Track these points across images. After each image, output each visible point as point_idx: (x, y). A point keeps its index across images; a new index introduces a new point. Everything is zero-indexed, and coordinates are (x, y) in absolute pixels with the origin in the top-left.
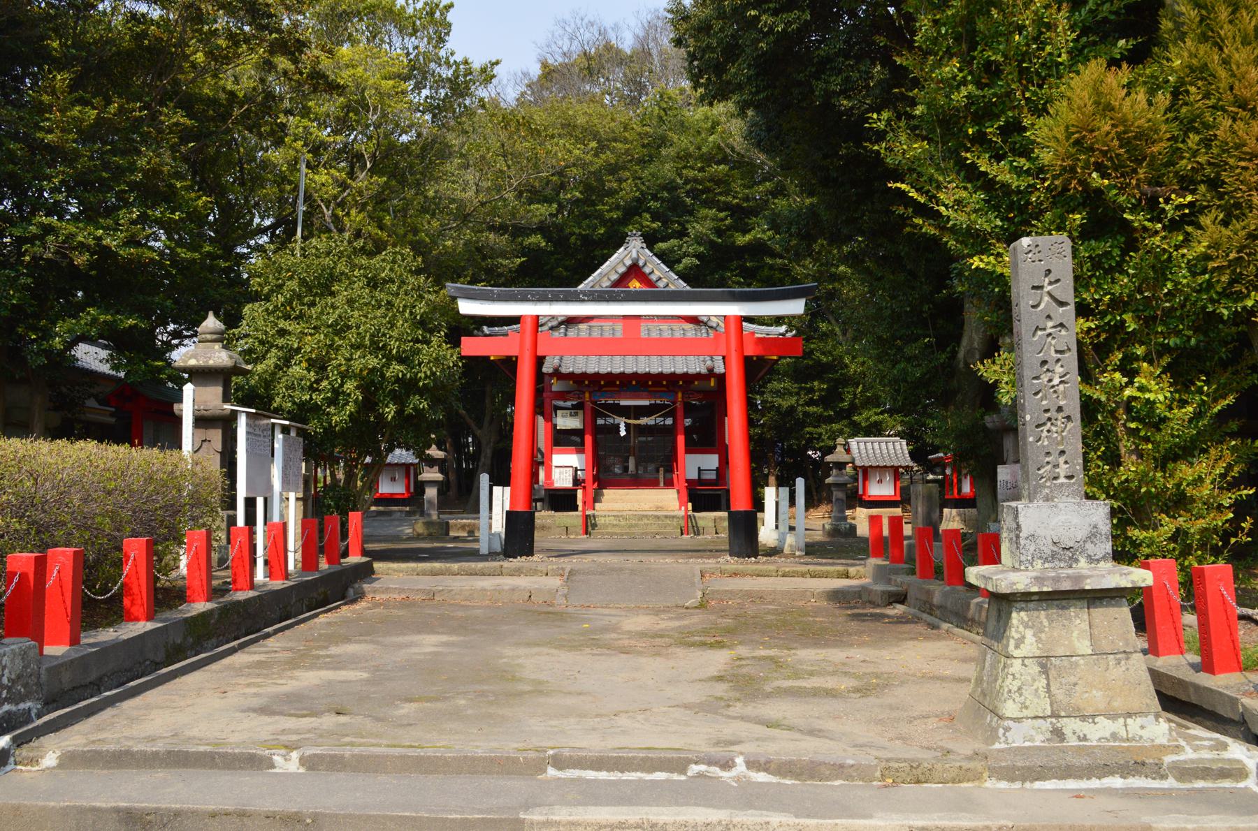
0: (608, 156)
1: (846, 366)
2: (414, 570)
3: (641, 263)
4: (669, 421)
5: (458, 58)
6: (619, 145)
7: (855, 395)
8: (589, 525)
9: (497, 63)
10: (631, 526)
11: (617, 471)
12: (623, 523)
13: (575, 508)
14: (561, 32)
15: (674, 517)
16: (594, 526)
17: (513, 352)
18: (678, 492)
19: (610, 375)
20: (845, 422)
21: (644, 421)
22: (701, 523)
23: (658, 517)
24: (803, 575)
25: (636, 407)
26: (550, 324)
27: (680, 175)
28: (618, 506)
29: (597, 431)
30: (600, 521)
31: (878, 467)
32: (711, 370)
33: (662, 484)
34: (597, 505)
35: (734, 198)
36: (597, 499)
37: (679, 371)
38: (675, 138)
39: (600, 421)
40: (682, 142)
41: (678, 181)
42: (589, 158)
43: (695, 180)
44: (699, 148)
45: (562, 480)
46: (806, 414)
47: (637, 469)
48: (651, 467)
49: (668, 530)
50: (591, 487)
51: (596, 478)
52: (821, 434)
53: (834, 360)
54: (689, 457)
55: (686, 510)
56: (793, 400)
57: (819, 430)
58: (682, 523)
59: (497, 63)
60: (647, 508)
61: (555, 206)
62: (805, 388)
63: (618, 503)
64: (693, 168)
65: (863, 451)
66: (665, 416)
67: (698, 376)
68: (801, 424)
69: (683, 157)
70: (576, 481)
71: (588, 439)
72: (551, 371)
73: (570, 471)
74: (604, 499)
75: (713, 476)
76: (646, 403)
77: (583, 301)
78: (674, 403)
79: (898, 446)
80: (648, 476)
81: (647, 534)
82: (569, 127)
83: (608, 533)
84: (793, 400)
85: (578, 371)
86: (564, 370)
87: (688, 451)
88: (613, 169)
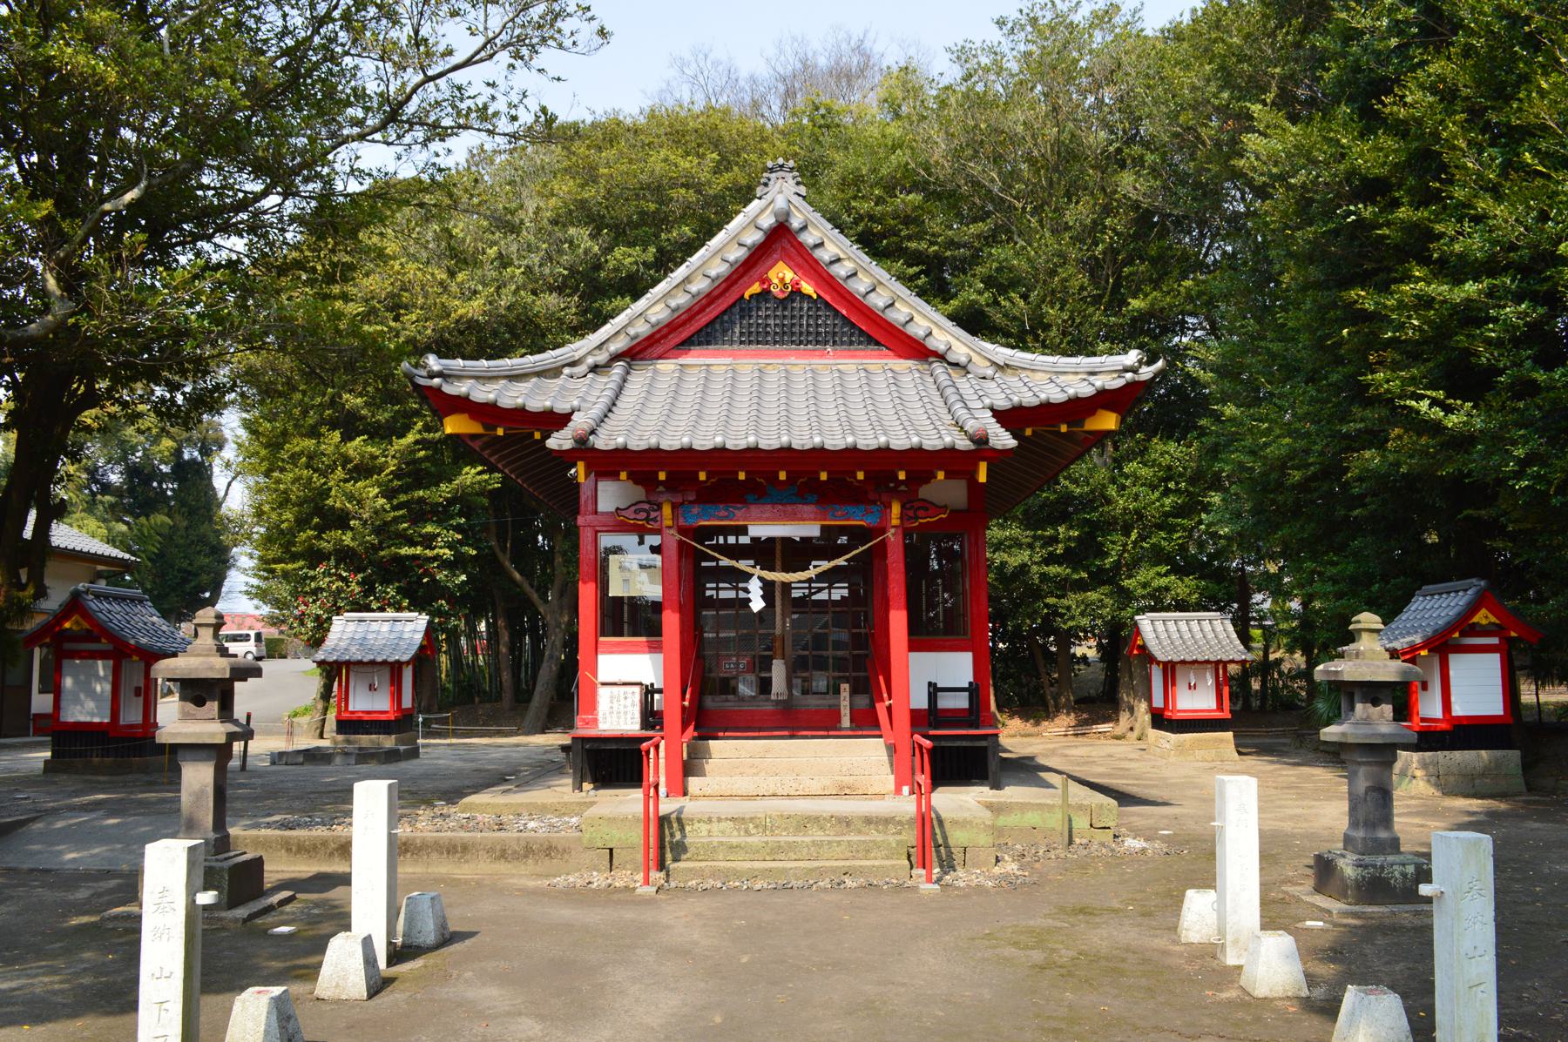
1: (1109, 501)
3: (795, 223)
8: (665, 842)
10: (777, 851)
16: (680, 849)
18: (892, 749)
20: (1106, 589)
23: (845, 822)
26: (590, 360)
27: (849, 210)
30: (695, 836)
31: (1195, 662)
32: (981, 440)
33: (846, 722)
34: (694, 783)
35: (932, 243)
36: (690, 767)
37: (900, 442)
41: (845, 216)
42: (704, 176)
43: (872, 218)
45: (614, 715)
46: (1044, 577)
47: (790, 685)
48: (820, 683)
52: (1069, 608)
53: (1092, 491)
56: (1023, 556)
57: (1065, 602)
58: (910, 837)
60: (815, 787)
61: (652, 249)
62: (1041, 537)
65: (1163, 636)
67: (948, 458)
68: (1037, 594)
70: (650, 717)
71: (671, 621)
74: (710, 765)
75: (961, 702)
76: (812, 530)
79: (1219, 628)
80: (813, 702)
81: (821, 872)
83: (715, 873)
84: (1023, 556)
85: (637, 444)
86: (602, 442)
87: (914, 646)
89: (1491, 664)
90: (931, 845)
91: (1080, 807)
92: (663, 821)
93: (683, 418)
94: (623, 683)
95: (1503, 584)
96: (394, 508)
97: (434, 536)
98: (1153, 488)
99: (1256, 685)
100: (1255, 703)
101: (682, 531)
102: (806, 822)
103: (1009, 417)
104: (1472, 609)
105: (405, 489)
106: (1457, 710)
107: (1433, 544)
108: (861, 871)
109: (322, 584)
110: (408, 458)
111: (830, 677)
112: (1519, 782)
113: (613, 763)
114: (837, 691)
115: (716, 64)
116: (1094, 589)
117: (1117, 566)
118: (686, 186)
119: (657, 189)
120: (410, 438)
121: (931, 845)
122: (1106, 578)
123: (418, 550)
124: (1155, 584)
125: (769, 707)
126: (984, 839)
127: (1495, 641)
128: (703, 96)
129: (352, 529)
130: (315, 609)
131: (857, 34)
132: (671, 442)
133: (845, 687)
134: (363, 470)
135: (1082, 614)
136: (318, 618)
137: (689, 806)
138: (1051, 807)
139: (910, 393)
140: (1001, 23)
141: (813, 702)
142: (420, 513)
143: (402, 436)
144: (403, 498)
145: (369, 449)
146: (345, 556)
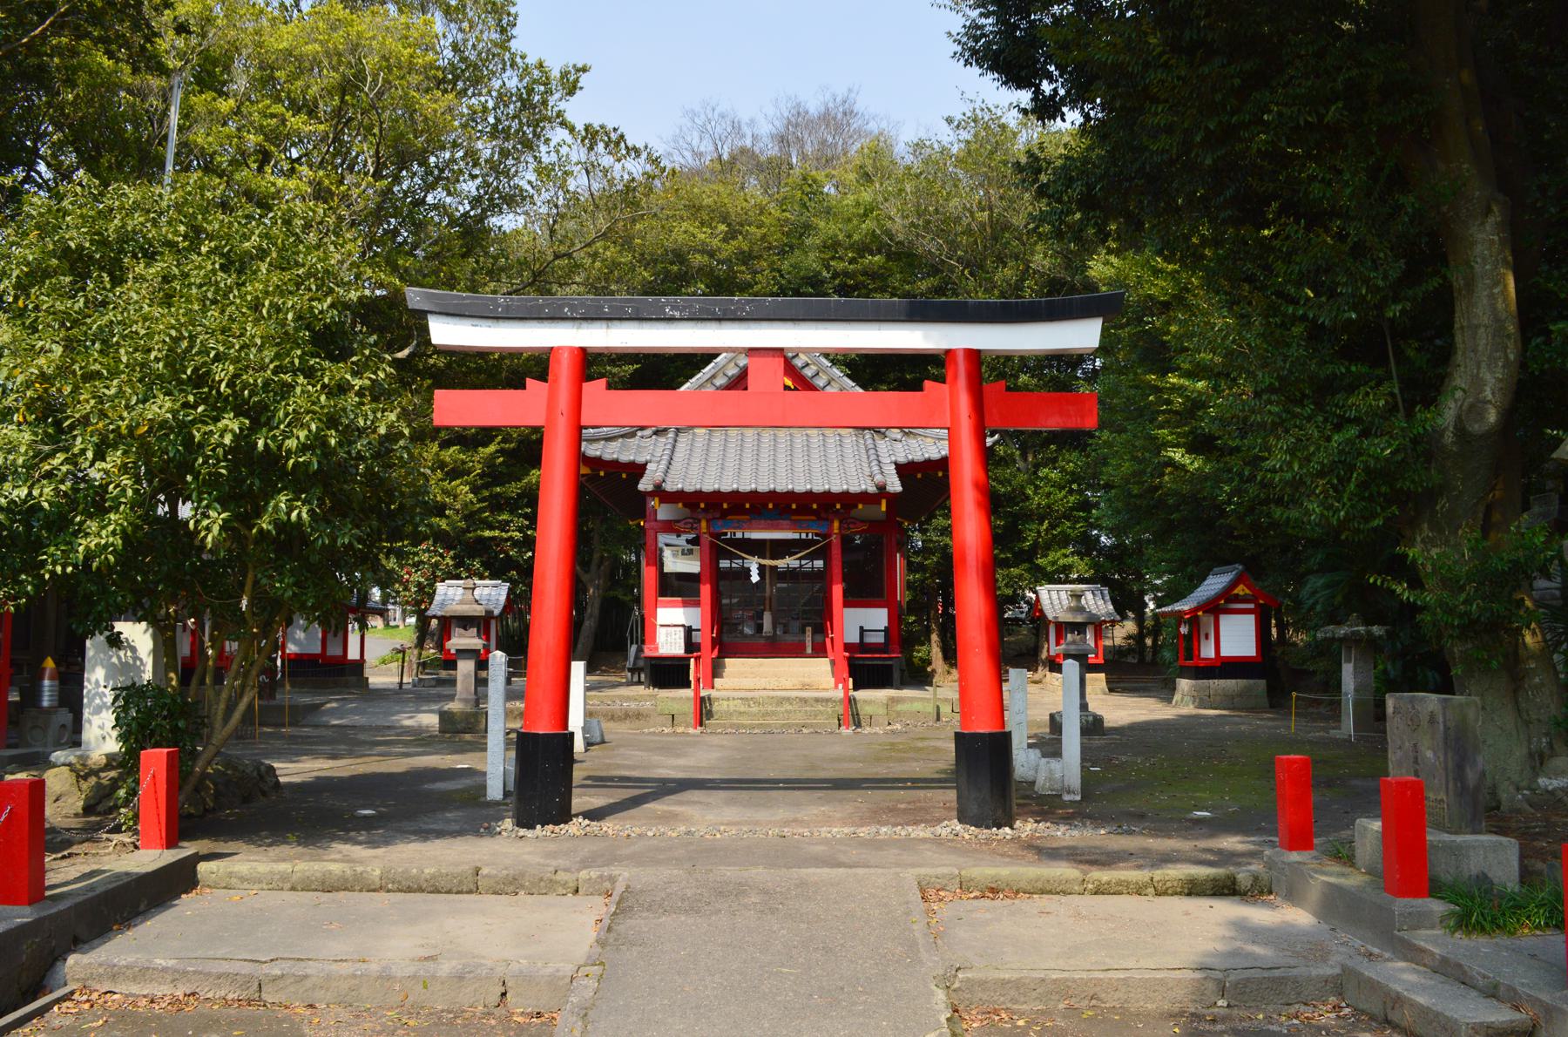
0: (739, 243)
1: (1027, 498)
2: (284, 877)
4: (819, 564)
5: (532, 60)
6: (753, 229)
7: (1039, 532)
8: (703, 710)
9: (584, 70)
10: (766, 715)
11: (748, 631)
12: (755, 709)
13: (688, 686)
14: (689, 124)
15: (828, 700)
16: (710, 715)
17: (537, 420)
18: (833, 663)
19: (735, 494)
20: (1026, 565)
21: (781, 563)
22: (865, 710)
23: (804, 701)
24: (1139, 891)
25: (772, 541)
27: (828, 267)
28: (747, 683)
29: (718, 577)
30: (715, 708)
32: (882, 488)
33: (809, 650)
36: (717, 671)
37: (837, 488)
38: (822, 224)
39: (724, 564)
40: (827, 228)
41: (825, 274)
42: (715, 243)
43: (846, 274)
44: (849, 236)
45: (669, 643)
47: (774, 627)
49: (820, 720)
50: (708, 654)
51: (715, 642)
53: (1014, 490)
54: (849, 612)
55: (846, 689)
58: (840, 709)
59: (584, 70)
60: (788, 685)
63: (746, 678)
64: (841, 258)
66: (812, 557)
67: (863, 496)
69: (832, 246)
70: (691, 646)
72: (650, 488)
73: (681, 632)
75: (880, 639)
77: (672, 319)
78: (825, 536)
80: (789, 638)
81: (789, 726)
82: (695, 209)
83: (731, 726)
85: (689, 488)
86: (669, 487)
88: (746, 258)
89: (1249, 622)
90: (852, 715)
91: (946, 700)
92: (702, 699)
93: (713, 470)
94: (671, 627)
95: (1253, 570)
96: (479, 501)
97: (507, 523)
98: (1061, 488)
99: (1149, 642)
100: (1149, 657)
101: (712, 535)
102: (781, 701)
103: (904, 470)
104: (1233, 584)
105: (486, 486)
106: (1223, 654)
107: (15, 703)
108: (811, 725)
109: (425, 557)
110: (489, 461)
111: (793, 624)
112: (1265, 701)
113: (669, 673)
114: (804, 632)
115: (723, 116)
116: (1016, 566)
117: (1035, 545)
118: (703, 252)
119: (679, 256)
120: (492, 448)
121: (852, 715)
122: (1027, 557)
123: (497, 533)
124: (1061, 562)
125: (762, 641)
126: (882, 711)
127: (1252, 606)
128: (711, 148)
129: (447, 517)
130: (417, 577)
131: (841, 93)
132: (708, 487)
133: (809, 629)
134: (455, 473)
135: (1006, 585)
136: (419, 584)
137: (714, 693)
138: (928, 700)
139: (848, 451)
140: (949, 121)
141: (789, 638)
142: (497, 504)
143: (485, 445)
144: (486, 493)
145: (462, 456)
146: (440, 537)
